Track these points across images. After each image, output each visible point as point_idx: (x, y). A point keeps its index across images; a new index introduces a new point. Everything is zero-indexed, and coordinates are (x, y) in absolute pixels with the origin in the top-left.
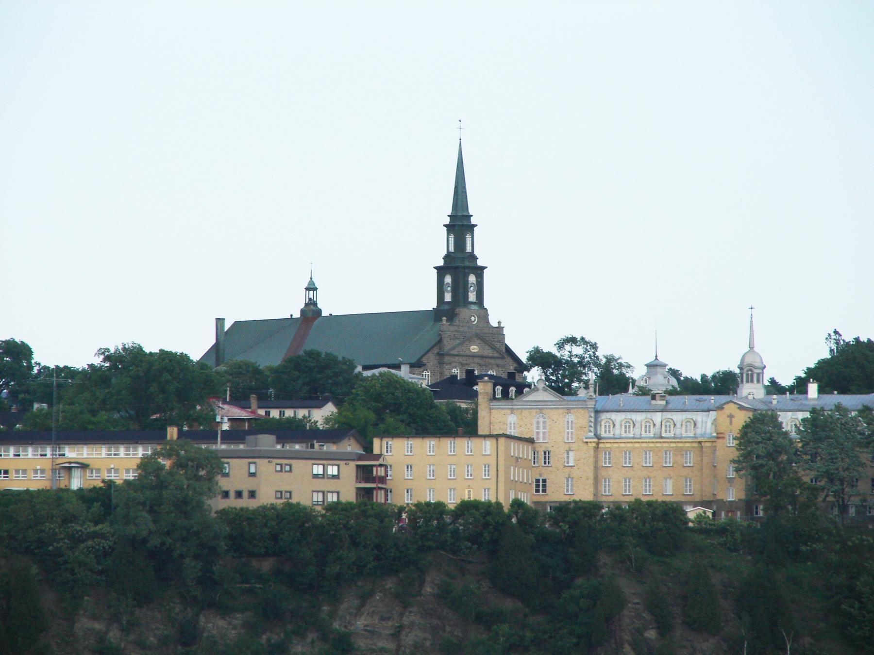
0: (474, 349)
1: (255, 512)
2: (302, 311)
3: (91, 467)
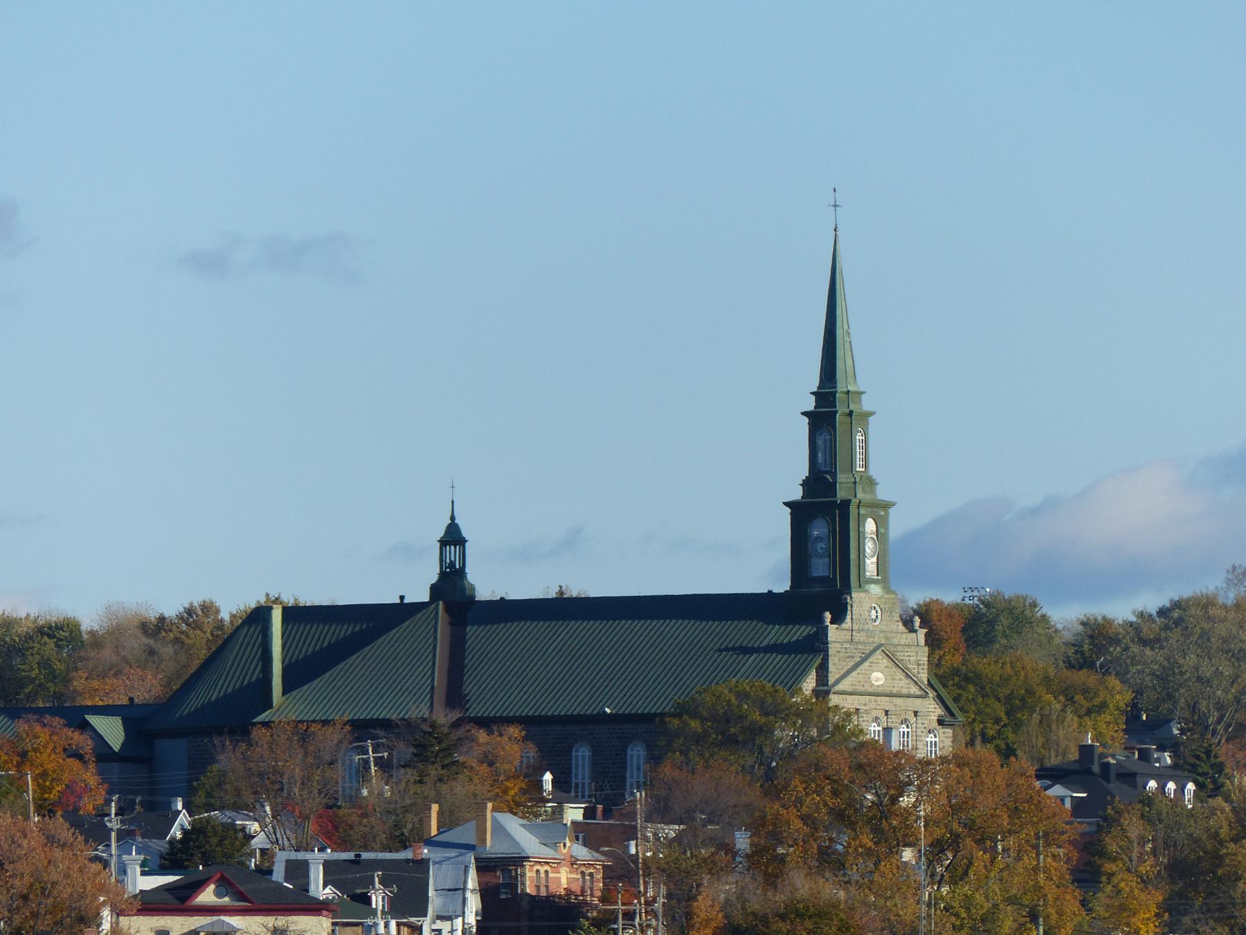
0: (878, 678)
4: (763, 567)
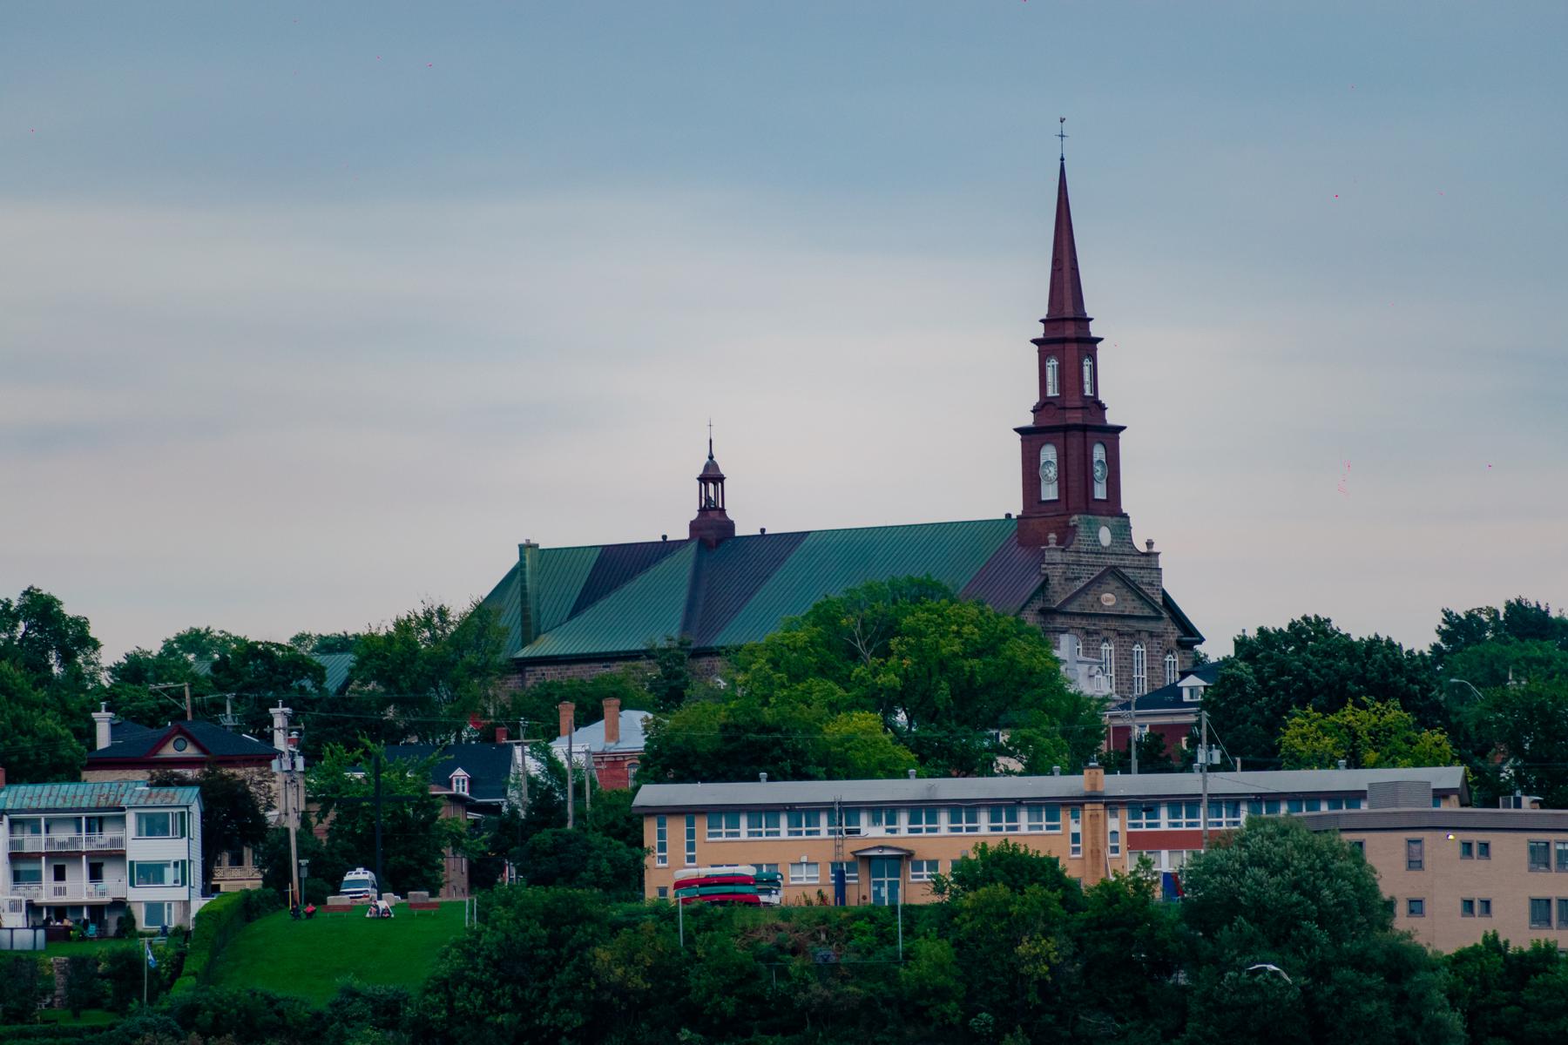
0: (1109, 600)
1: (69, 986)
2: (694, 526)
3: (917, 857)
4: (994, 492)
